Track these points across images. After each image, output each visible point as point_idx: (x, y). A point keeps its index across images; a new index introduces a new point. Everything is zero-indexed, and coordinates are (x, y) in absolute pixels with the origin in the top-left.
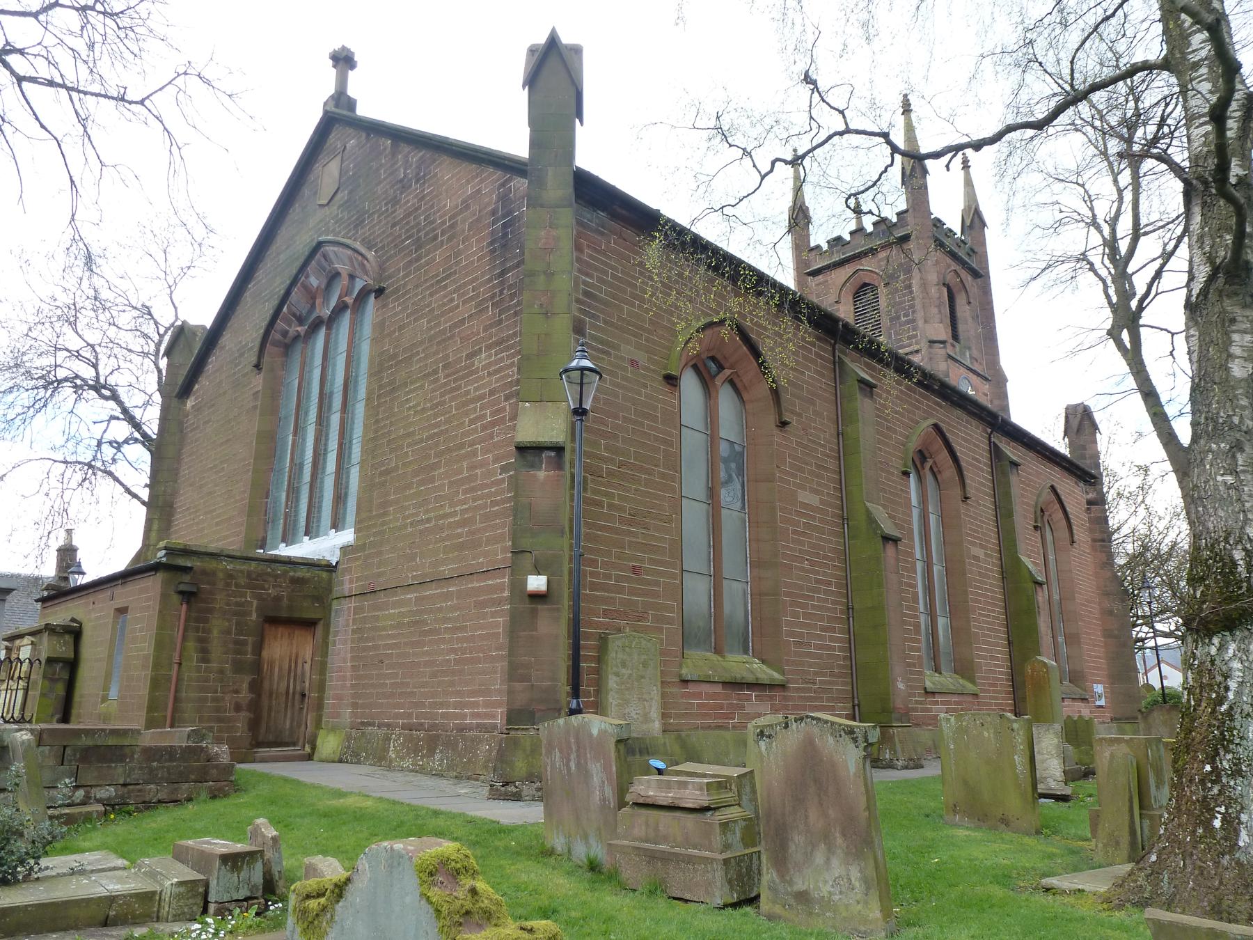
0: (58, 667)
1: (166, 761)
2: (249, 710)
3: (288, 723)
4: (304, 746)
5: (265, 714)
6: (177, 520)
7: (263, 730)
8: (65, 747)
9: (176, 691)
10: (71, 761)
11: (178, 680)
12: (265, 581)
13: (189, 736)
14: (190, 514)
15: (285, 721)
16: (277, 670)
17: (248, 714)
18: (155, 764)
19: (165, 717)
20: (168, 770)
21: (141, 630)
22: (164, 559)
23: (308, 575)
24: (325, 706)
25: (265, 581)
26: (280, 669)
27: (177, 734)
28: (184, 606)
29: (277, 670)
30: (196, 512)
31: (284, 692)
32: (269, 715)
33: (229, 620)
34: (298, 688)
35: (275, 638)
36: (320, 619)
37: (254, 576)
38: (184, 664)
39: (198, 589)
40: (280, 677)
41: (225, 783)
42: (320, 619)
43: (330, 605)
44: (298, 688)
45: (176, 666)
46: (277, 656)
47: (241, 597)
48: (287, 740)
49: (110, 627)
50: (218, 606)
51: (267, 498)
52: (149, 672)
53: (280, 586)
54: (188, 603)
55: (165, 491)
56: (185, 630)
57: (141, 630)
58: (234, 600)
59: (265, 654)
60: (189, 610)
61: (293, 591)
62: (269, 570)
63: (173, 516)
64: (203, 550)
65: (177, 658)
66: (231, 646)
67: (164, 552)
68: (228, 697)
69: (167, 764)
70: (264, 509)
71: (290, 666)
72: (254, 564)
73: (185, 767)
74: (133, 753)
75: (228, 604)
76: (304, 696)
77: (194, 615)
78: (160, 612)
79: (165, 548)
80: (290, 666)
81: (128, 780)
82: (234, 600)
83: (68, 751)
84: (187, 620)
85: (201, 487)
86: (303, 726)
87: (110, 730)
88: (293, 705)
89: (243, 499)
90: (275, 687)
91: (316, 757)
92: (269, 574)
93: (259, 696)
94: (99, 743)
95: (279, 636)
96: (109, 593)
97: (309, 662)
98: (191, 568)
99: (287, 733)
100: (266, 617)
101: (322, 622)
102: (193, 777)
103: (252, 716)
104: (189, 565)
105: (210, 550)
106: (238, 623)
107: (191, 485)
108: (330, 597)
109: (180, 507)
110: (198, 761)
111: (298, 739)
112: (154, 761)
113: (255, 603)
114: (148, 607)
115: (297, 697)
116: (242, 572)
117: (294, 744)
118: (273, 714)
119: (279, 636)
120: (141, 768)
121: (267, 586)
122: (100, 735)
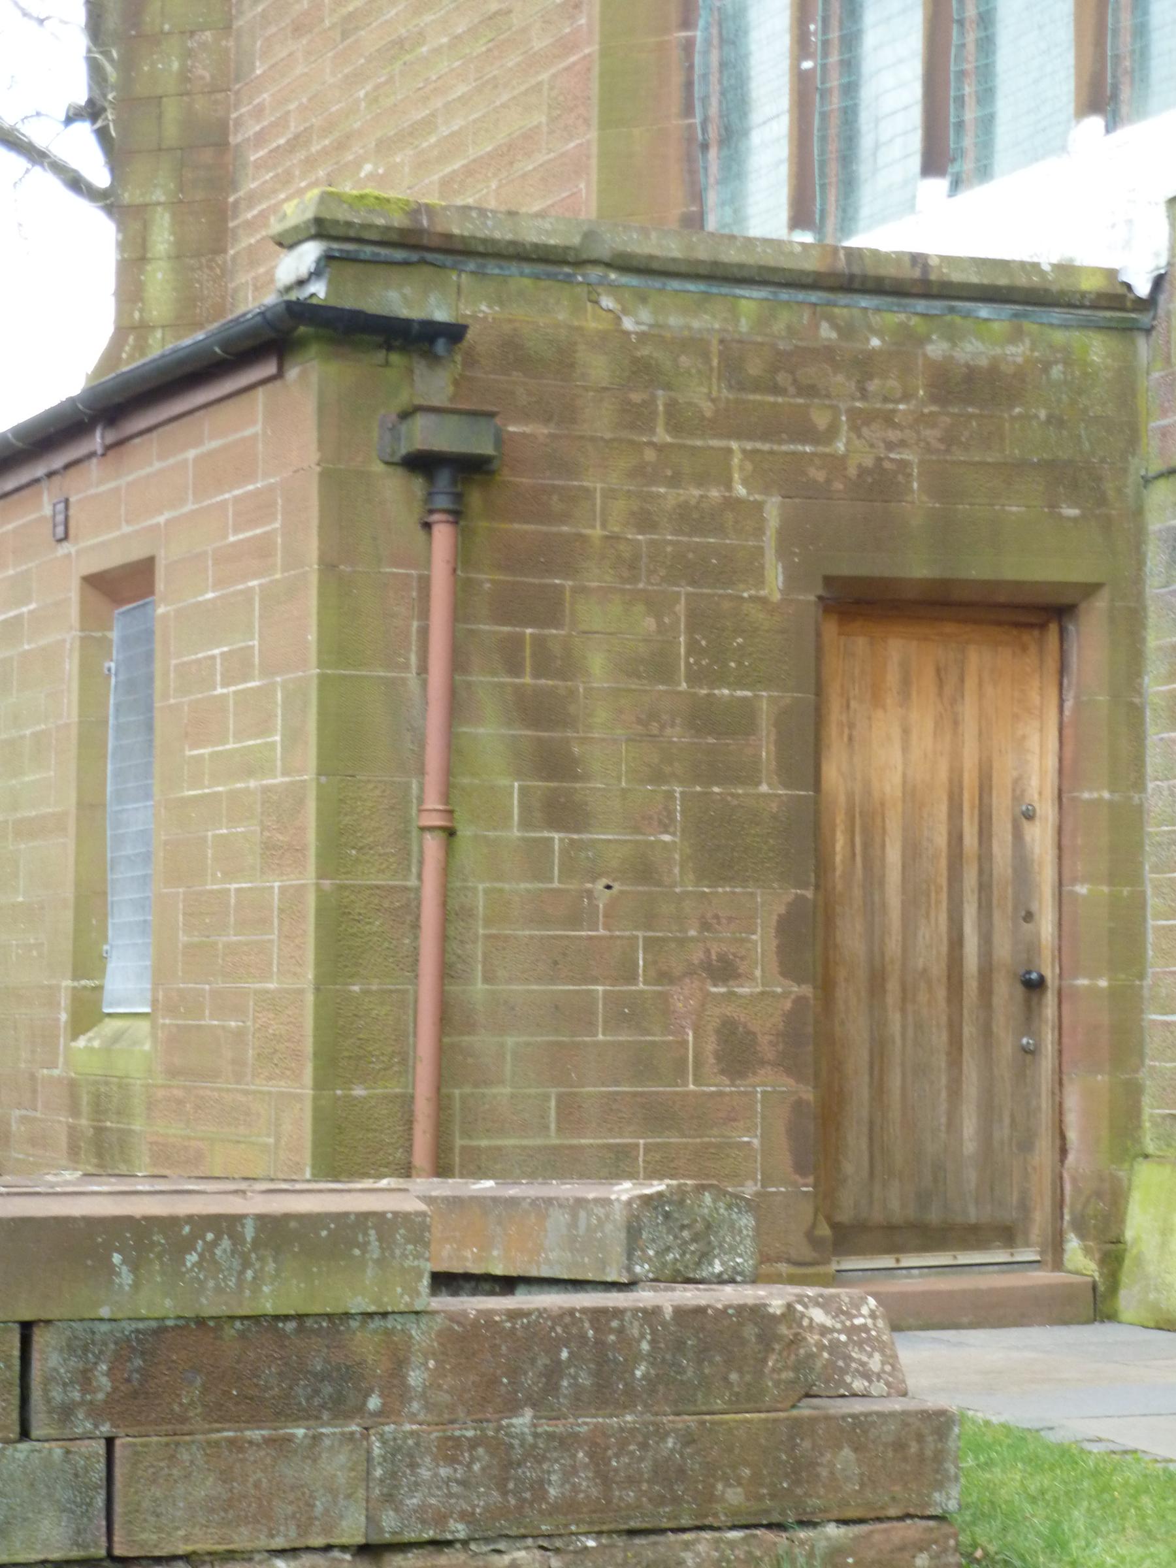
0: (824, 392)
1: (579, 1403)
2: (789, 1064)
3: (969, 1127)
4: (1056, 1247)
5: (860, 1089)
6: (252, 199)
7: (854, 1165)
8: (27, 1328)
9: (447, 972)
10: (66, 1412)
11: (448, 915)
12: (809, 391)
13: (633, 1232)
14: (310, 163)
15: (953, 1124)
16: (893, 855)
17: (786, 1084)
18: (523, 1421)
19: (407, 1101)
20: (598, 1457)
21: (238, 666)
22: (319, 290)
23: (1017, 352)
24: (1153, 1043)
25: (809, 391)
26: (913, 851)
27: (558, 1218)
28: (443, 534)
29: (893, 855)
30: (341, 146)
31: (938, 970)
32: (879, 1090)
33: (656, 605)
34: (1003, 950)
35: (876, 698)
36: (1091, 589)
37: (754, 368)
38: (466, 832)
39: (499, 440)
40: (914, 899)
41: (911, 1530)
42: (1091, 589)
43: (1138, 512)
44: (1003, 950)
45: (432, 845)
46: (890, 785)
47: (701, 480)
48: (973, 1215)
49: (71, 666)
50: (597, 532)
51: (687, 23)
52: (309, 876)
53: (888, 419)
54: (457, 515)
55: (185, 76)
56: (458, 662)
57: (238, 666)
58: (669, 496)
59: (833, 773)
60: (463, 557)
61: (950, 440)
62: (827, 332)
63: (234, 185)
64: (502, 233)
65: (433, 802)
66: (677, 735)
67: (310, 253)
68: (683, 998)
69: (585, 1424)
70: (677, 79)
71: (956, 839)
72: (750, 300)
73: (688, 1439)
74: (400, 1364)
75: (645, 522)
76: (1034, 986)
77: (487, 579)
78: (328, 567)
79: (321, 229)
80: (956, 839)
81: (390, 1524)
82: (669, 496)
83: (40, 1338)
84: (460, 612)
85: (349, 25)
86: (1044, 1146)
87: (265, 1221)
88: (987, 1033)
89: (566, 46)
90: (893, 945)
91: (1128, 1301)
92: (828, 353)
93: (826, 987)
94: (210, 1305)
95: (893, 677)
96: (46, 504)
97: (1047, 811)
98: (454, 333)
99: (971, 1176)
100: (829, 581)
101: (1101, 603)
102: (734, 1496)
103: (808, 1094)
104: (441, 315)
105: (531, 234)
106: (696, 621)
107: (298, 29)
108: (1138, 467)
109: (260, 139)
110: (751, 1398)
111: (1024, 1207)
112: (513, 1408)
113: (773, 510)
114: (262, 549)
115: (1005, 991)
116: (694, 344)
117: (1008, 1235)
118: (895, 1081)
119: (893, 677)
120: (450, 1449)
121: (821, 420)
122: (208, 1260)
